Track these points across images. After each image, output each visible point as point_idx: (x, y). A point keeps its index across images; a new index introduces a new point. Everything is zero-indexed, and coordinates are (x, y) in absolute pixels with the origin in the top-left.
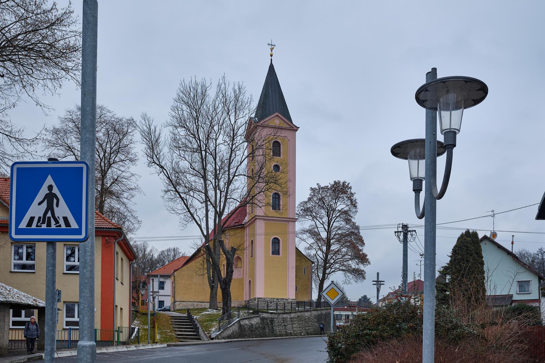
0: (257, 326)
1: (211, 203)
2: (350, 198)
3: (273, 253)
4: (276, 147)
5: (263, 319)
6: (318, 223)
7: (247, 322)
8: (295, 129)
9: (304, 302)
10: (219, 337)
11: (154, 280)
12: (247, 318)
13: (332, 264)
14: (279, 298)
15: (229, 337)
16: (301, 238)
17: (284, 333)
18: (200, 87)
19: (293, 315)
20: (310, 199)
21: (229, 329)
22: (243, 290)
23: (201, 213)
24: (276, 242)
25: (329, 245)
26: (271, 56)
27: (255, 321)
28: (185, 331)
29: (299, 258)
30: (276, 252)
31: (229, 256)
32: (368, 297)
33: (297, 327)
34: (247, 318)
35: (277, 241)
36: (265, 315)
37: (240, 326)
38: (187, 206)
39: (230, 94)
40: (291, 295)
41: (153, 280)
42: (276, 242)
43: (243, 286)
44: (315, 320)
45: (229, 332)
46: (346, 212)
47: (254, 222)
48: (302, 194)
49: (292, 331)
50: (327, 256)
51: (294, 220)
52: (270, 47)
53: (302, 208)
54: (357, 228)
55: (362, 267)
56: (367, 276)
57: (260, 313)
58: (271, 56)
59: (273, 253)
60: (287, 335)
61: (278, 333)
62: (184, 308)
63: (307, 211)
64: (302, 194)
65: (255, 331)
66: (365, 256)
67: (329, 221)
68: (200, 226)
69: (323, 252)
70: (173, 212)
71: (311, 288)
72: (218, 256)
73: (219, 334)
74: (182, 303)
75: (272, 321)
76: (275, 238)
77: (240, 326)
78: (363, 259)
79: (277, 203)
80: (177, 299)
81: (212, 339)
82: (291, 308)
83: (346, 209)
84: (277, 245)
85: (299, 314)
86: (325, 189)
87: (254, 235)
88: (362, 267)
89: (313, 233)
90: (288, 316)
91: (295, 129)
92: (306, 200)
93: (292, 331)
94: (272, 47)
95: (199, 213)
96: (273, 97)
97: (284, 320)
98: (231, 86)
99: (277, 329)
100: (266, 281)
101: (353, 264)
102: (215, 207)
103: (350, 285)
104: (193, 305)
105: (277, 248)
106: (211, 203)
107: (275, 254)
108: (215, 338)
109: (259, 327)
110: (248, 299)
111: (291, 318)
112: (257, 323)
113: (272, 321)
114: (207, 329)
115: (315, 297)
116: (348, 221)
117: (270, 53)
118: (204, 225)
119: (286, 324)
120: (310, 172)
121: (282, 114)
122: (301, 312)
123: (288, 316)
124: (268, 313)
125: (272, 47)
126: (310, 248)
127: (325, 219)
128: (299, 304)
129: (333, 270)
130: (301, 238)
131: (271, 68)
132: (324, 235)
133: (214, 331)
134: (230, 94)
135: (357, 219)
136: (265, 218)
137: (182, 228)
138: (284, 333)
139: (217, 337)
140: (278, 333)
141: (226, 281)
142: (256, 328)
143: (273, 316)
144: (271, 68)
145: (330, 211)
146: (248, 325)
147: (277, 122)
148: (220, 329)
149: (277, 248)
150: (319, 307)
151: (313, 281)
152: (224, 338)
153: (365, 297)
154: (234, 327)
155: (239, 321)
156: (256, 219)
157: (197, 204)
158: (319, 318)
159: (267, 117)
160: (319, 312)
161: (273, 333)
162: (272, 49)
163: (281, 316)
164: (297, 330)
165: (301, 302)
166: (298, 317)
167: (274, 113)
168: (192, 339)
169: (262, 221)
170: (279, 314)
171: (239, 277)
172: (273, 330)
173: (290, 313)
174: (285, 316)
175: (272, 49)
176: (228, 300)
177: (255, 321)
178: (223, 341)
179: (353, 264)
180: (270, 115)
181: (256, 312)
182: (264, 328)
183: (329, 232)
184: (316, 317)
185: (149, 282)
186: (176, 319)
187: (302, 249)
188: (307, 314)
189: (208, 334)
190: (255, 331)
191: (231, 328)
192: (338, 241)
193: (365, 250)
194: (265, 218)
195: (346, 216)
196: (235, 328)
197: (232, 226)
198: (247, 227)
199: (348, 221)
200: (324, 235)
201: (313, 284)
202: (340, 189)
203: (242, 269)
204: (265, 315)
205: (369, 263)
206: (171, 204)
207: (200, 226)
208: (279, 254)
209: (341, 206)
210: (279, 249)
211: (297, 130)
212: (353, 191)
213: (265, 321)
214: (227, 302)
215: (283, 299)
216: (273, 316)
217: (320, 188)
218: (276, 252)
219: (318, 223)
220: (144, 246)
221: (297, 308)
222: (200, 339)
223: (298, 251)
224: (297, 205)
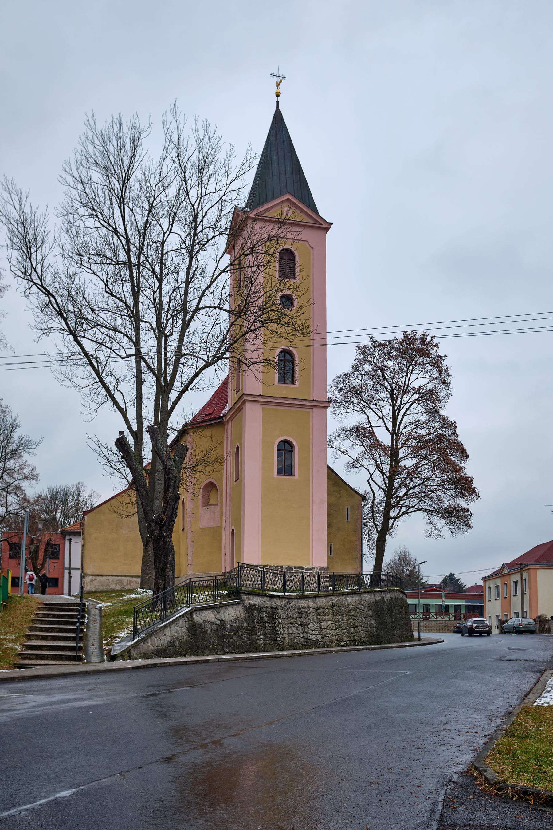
0: (236, 625)
1: (150, 368)
2: (437, 363)
3: (281, 472)
4: (287, 262)
5: (250, 610)
6: (373, 417)
7: (210, 616)
8: (324, 227)
9: (347, 576)
10: (134, 653)
11: (73, 541)
12: (211, 608)
13: (401, 498)
14: (292, 564)
15: (161, 653)
16: (338, 449)
17: (302, 641)
18: (125, 130)
19: (320, 602)
20: (356, 368)
21: (161, 634)
22: (220, 550)
23: (128, 390)
24: (286, 448)
25: (395, 460)
26: (278, 96)
27: (232, 614)
28: (54, 638)
29: (335, 488)
30: (286, 469)
31: (170, 463)
32: (457, 576)
33: (329, 628)
34: (211, 608)
35: (287, 447)
36: (256, 601)
37: (193, 628)
38: (97, 371)
39: (192, 156)
40: (317, 558)
41: (70, 540)
42: (286, 448)
43: (221, 543)
44: (370, 613)
45: (162, 640)
46: (431, 392)
47: (240, 408)
48: (339, 360)
49: (319, 637)
50: (391, 481)
51: (324, 404)
52: (276, 79)
53: (340, 386)
54: (452, 426)
55: (462, 503)
56: (474, 521)
57: (244, 597)
58: (278, 96)
59: (281, 472)
60: (307, 646)
61: (287, 642)
62: (101, 588)
63: (353, 394)
64: (339, 360)
65: (230, 636)
66: (468, 481)
67: (394, 411)
68: (123, 413)
69: (383, 474)
70: (69, 384)
71: (361, 554)
72: (160, 476)
73: (133, 646)
74: (98, 578)
75: (273, 613)
76: (285, 442)
77: (193, 628)
78: (465, 486)
79: (288, 370)
80: (88, 571)
81: (113, 658)
82: (318, 586)
83: (431, 386)
84: (288, 455)
85: (335, 599)
86: (388, 344)
87: (240, 436)
88: (462, 503)
89: (363, 433)
90: (311, 604)
91: (324, 227)
92: (348, 369)
93: (319, 637)
94: (280, 79)
95: (123, 386)
96: (279, 152)
97: (301, 612)
98: (191, 123)
99: (285, 633)
100: (269, 532)
101: (447, 499)
102: (157, 376)
103: (440, 538)
104: (121, 582)
105: (288, 462)
106: (150, 368)
107: (284, 474)
108: (123, 656)
109: (240, 628)
110: (228, 569)
111: (318, 608)
112: (237, 619)
113: (273, 613)
114: (108, 630)
115: (368, 567)
116: (433, 412)
117: (275, 89)
118: (132, 413)
119: (306, 621)
120: (355, 309)
121: (297, 198)
122: (339, 595)
123: (311, 604)
124: (263, 596)
125: (280, 79)
126: (356, 463)
127: (387, 410)
128: (334, 579)
129: (404, 509)
130: (338, 449)
131: (278, 120)
132: (385, 438)
133: (123, 639)
134: (192, 156)
135: (449, 410)
136: (263, 401)
137: (88, 418)
138: (302, 641)
139: (127, 654)
140: (287, 642)
141: (162, 520)
142: (232, 630)
143: (275, 603)
144: (278, 120)
145: (397, 393)
146: (213, 623)
147: (287, 212)
148: (135, 633)
149: (288, 462)
150: (377, 586)
151: (364, 541)
152: (146, 656)
153: (451, 577)
154: (174, 628)
155: (190, 613)
156: (245, 401)
157: (121, 369)
158: (377, 609)
159: (267, 201)
160: (378, 597)
161: (275, 642)
162: (278, 85)
163: (293, 603)
164: (332, 635)
165: (341, 577)
166: (333, 605)
167: (281, 195)
168: (60, 658)
169: (257, 406)
170: (290, 598)
171: (212, 524)
172: (276, 635)
173: (315, 597)
174: (303, 603)
175: (278, 85)
176: (166, 564)
177: (232, 614)
178: (140, 662)
179: (447, 499)
180: (274, 198)
181: (236, 594)
182: (254, 630)
183: (395, 434)
184: (370, 606)
185: (64, 544)
186: (52, 610)
187: (339, 468)
188: (352, 600)
189: (107, 645)
190: (230, 636)
191: (167, 631)
192: (415, 451)
193: (470, 469)
194: (263, 401)
195: (430, 398)
196: (179, 630)
197: (199, 423)
198: (228, 422)
199: (433, 412)
200: (385, 438)
201: (365, 546)
202: (416, 349)
203: (218, 508)
204: (256, 601)
205: (478, 497)
206: (65, 369)
207: (123, 413)
208: (292, 473)
209: (419, 379)
210: (292, 465)
211: (327, 229)
212: (441, 352)
213: (256, 613)
214: (164, 568)
215: (302, 568)
216: (275, 603)
217: (376, 345)
218: (286, 469)
219: (373, 417)
220: (77, 489)
221: (331, 588)
222: (80, 659)
223: (332, 475)
224: (329, 381)
